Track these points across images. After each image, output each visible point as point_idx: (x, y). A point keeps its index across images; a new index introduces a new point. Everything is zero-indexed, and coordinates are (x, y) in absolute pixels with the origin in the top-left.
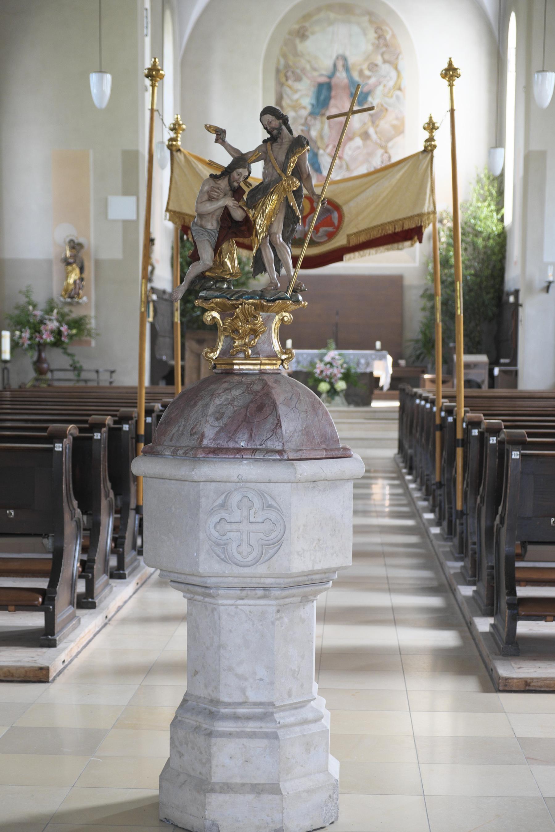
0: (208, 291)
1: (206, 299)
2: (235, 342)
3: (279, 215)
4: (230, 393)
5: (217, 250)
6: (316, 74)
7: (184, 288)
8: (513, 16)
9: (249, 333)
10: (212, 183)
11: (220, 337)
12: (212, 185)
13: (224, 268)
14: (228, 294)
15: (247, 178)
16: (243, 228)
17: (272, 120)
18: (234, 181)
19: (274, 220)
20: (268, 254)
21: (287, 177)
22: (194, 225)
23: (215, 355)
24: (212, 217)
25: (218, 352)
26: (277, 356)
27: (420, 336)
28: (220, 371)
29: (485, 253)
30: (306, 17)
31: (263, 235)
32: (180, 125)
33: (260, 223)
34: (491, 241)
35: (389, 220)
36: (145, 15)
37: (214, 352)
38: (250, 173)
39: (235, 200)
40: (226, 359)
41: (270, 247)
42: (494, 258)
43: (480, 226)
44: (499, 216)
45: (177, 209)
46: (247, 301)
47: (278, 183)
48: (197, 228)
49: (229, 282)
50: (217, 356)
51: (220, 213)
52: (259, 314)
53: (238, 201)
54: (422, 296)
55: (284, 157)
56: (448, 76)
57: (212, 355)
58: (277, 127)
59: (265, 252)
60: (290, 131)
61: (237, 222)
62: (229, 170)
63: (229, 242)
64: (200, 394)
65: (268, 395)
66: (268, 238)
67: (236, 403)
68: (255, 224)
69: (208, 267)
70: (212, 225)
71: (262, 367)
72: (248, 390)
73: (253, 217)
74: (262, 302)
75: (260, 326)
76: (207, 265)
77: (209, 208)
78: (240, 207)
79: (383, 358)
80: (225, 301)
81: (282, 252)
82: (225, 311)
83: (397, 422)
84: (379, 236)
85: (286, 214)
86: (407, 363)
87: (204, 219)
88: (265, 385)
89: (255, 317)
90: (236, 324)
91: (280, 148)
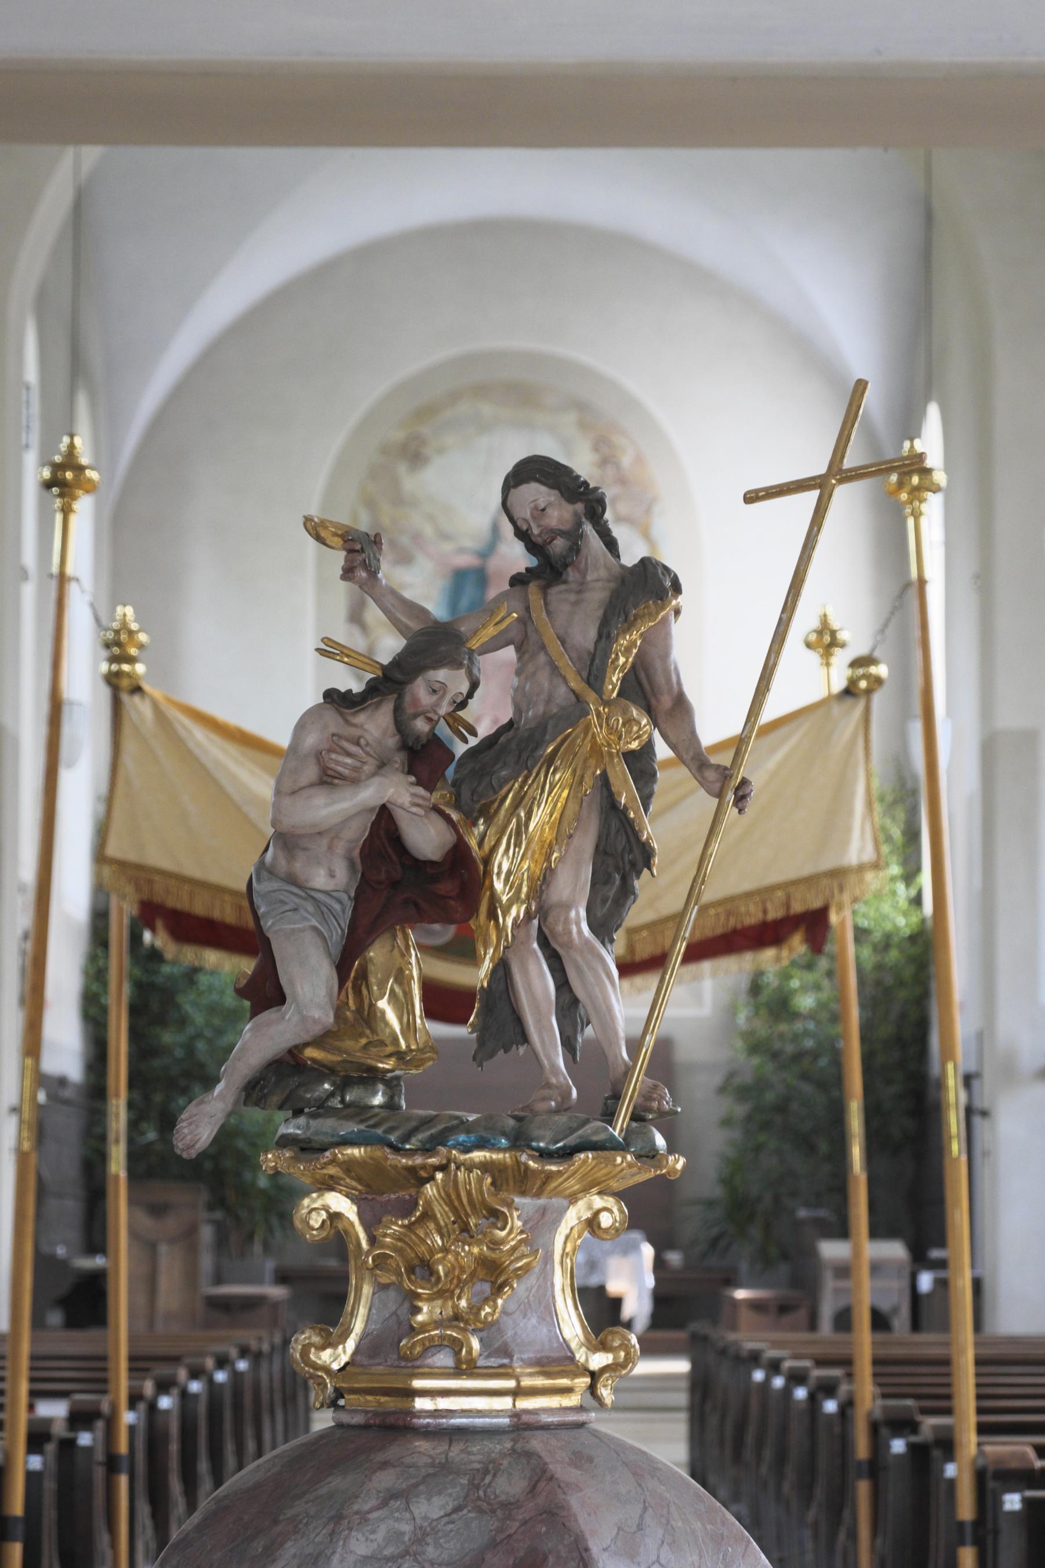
0: (314, 1116)
1: (306, 1148)
2: (418, 1310)
3: (576, 841)
4: (407, 1509)
5: (348, 964)
6: (447, 547)
7: (220, 1105)
8: (933, 414)
9: (473, 1275)
10: (333, 721)
11: (359, 1290)
12: (333, 729)
13: (374, 1031)
14: (391, 1130)
15: (463, 705)
16: (446, 887)
17: (550, 504)
18: (416, 716)
19: (560, 859)
20: (536, 982)
21: (607, 703)
22: (265, 874)
23: (336, 1357)
24: (330, 848)
25: (351, 1344)
26: (572, 1359)
27: (718, 1192)
28: (358, 1419)
29: (878, 983)
30: (426, 413)
31: (517, 911)
32: (131, 633)
33: (507, 869)
34: (894, 955)
35: (747, 886)
36: (24, 398)
37: (333, 1345)
38: (474, 686)
39: (419, 783)
40: (380, 1373)
41: (540, 954)
42: (902, 994)
43: (865, 916)
44: (913, 892)
45: (131, 856)
46: (463, 1157)
47: (573, 724)
48: (275, 885)
49: (392, 1085)
50: (345, 1359)
51: (358, 831)
52: (510, 1205)
53: (430, 788)
54: (722, 1090)
55: (592, 634)
56: (907, 488)
57: (326, 1356)
58: (566, 527)
59: (525, 972)
60: (611, 544)
61: (420, 865)
62: (399, 676)
63: (394, 937)
64: (289, 1513)
65: (555, 1516)
66: (536, 922)
67: (431, 1552)
68: (487, 873)
69: (317, 1030)
70: (330, 876)
71: (526, 1404)
72: (476, 1497)
73: (480, 844)
74: (524, 1158)
75: (514, 1249)
76: (315, 1022)
77: (324, 812)
78: (436, 809)
79: (631, 1249)
80: (380, 1152)
81: (589, 975)
82: (379, 1192)
83: (683, 1416)
84: (719, 931)
85: (600, 837)
86: (687, 1258)
87: (301, 857)
88: (541, 1476)
89: (496, 1217)
90: (423, 1241)
91: (576, 604)
